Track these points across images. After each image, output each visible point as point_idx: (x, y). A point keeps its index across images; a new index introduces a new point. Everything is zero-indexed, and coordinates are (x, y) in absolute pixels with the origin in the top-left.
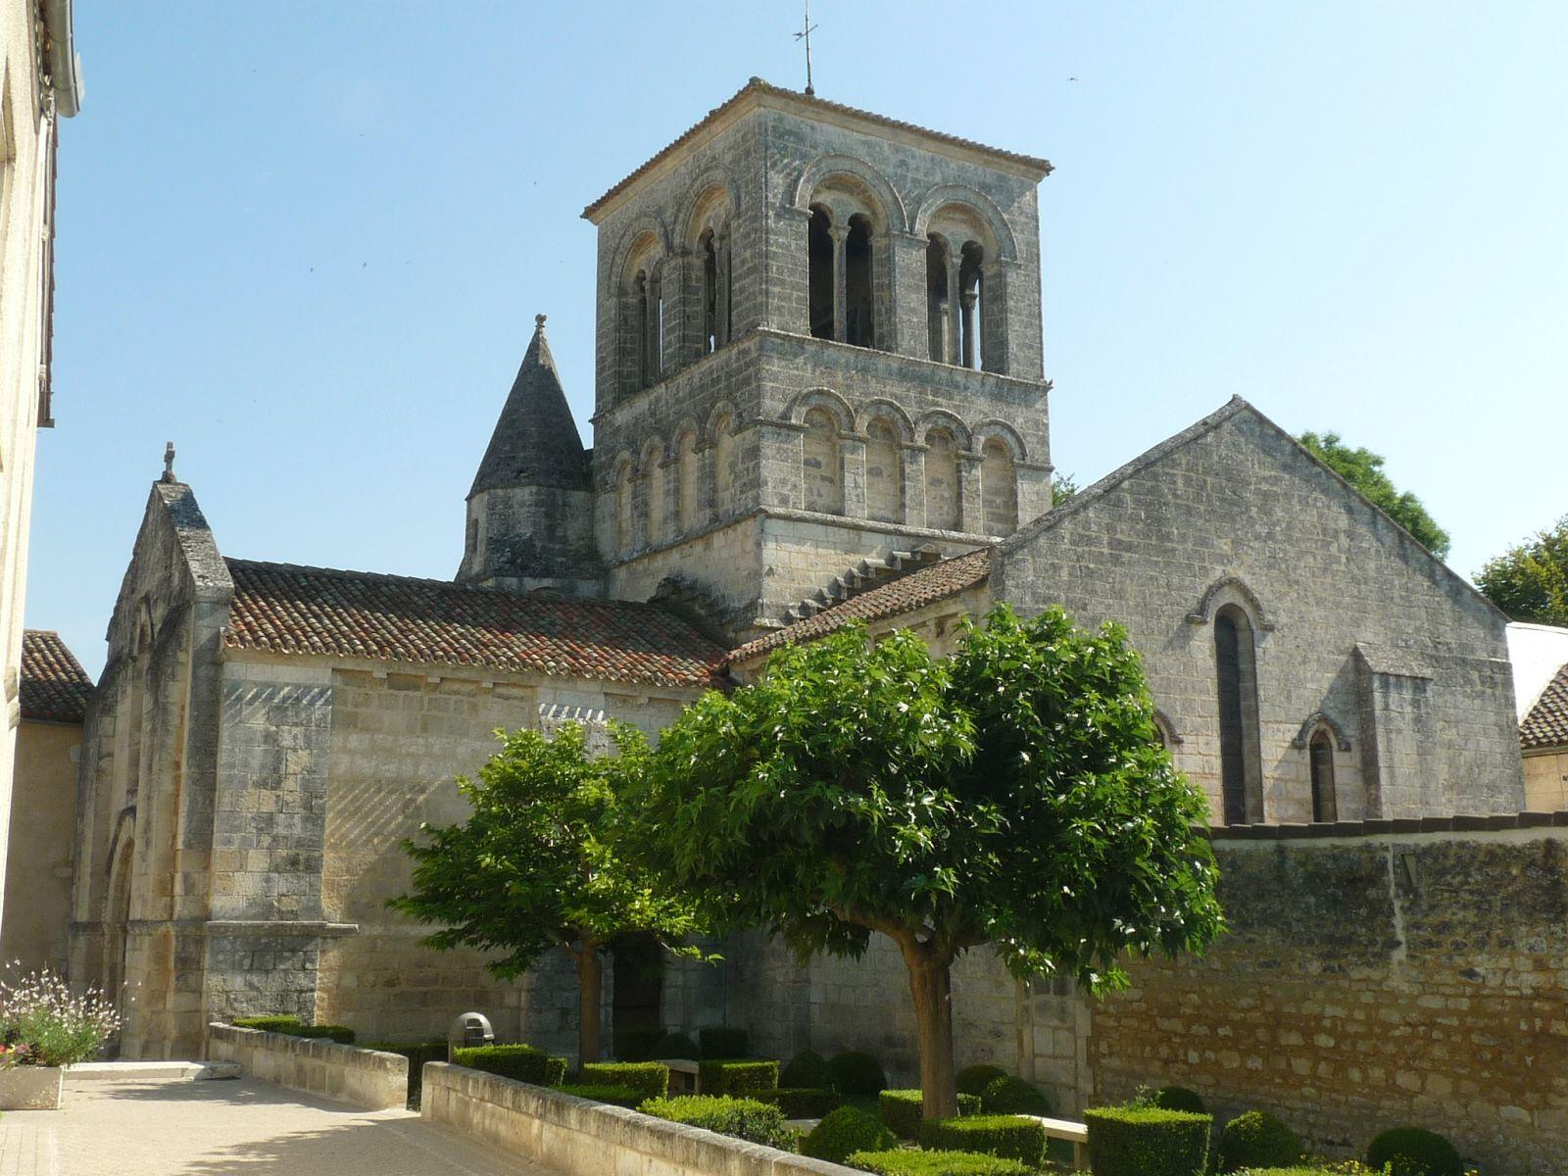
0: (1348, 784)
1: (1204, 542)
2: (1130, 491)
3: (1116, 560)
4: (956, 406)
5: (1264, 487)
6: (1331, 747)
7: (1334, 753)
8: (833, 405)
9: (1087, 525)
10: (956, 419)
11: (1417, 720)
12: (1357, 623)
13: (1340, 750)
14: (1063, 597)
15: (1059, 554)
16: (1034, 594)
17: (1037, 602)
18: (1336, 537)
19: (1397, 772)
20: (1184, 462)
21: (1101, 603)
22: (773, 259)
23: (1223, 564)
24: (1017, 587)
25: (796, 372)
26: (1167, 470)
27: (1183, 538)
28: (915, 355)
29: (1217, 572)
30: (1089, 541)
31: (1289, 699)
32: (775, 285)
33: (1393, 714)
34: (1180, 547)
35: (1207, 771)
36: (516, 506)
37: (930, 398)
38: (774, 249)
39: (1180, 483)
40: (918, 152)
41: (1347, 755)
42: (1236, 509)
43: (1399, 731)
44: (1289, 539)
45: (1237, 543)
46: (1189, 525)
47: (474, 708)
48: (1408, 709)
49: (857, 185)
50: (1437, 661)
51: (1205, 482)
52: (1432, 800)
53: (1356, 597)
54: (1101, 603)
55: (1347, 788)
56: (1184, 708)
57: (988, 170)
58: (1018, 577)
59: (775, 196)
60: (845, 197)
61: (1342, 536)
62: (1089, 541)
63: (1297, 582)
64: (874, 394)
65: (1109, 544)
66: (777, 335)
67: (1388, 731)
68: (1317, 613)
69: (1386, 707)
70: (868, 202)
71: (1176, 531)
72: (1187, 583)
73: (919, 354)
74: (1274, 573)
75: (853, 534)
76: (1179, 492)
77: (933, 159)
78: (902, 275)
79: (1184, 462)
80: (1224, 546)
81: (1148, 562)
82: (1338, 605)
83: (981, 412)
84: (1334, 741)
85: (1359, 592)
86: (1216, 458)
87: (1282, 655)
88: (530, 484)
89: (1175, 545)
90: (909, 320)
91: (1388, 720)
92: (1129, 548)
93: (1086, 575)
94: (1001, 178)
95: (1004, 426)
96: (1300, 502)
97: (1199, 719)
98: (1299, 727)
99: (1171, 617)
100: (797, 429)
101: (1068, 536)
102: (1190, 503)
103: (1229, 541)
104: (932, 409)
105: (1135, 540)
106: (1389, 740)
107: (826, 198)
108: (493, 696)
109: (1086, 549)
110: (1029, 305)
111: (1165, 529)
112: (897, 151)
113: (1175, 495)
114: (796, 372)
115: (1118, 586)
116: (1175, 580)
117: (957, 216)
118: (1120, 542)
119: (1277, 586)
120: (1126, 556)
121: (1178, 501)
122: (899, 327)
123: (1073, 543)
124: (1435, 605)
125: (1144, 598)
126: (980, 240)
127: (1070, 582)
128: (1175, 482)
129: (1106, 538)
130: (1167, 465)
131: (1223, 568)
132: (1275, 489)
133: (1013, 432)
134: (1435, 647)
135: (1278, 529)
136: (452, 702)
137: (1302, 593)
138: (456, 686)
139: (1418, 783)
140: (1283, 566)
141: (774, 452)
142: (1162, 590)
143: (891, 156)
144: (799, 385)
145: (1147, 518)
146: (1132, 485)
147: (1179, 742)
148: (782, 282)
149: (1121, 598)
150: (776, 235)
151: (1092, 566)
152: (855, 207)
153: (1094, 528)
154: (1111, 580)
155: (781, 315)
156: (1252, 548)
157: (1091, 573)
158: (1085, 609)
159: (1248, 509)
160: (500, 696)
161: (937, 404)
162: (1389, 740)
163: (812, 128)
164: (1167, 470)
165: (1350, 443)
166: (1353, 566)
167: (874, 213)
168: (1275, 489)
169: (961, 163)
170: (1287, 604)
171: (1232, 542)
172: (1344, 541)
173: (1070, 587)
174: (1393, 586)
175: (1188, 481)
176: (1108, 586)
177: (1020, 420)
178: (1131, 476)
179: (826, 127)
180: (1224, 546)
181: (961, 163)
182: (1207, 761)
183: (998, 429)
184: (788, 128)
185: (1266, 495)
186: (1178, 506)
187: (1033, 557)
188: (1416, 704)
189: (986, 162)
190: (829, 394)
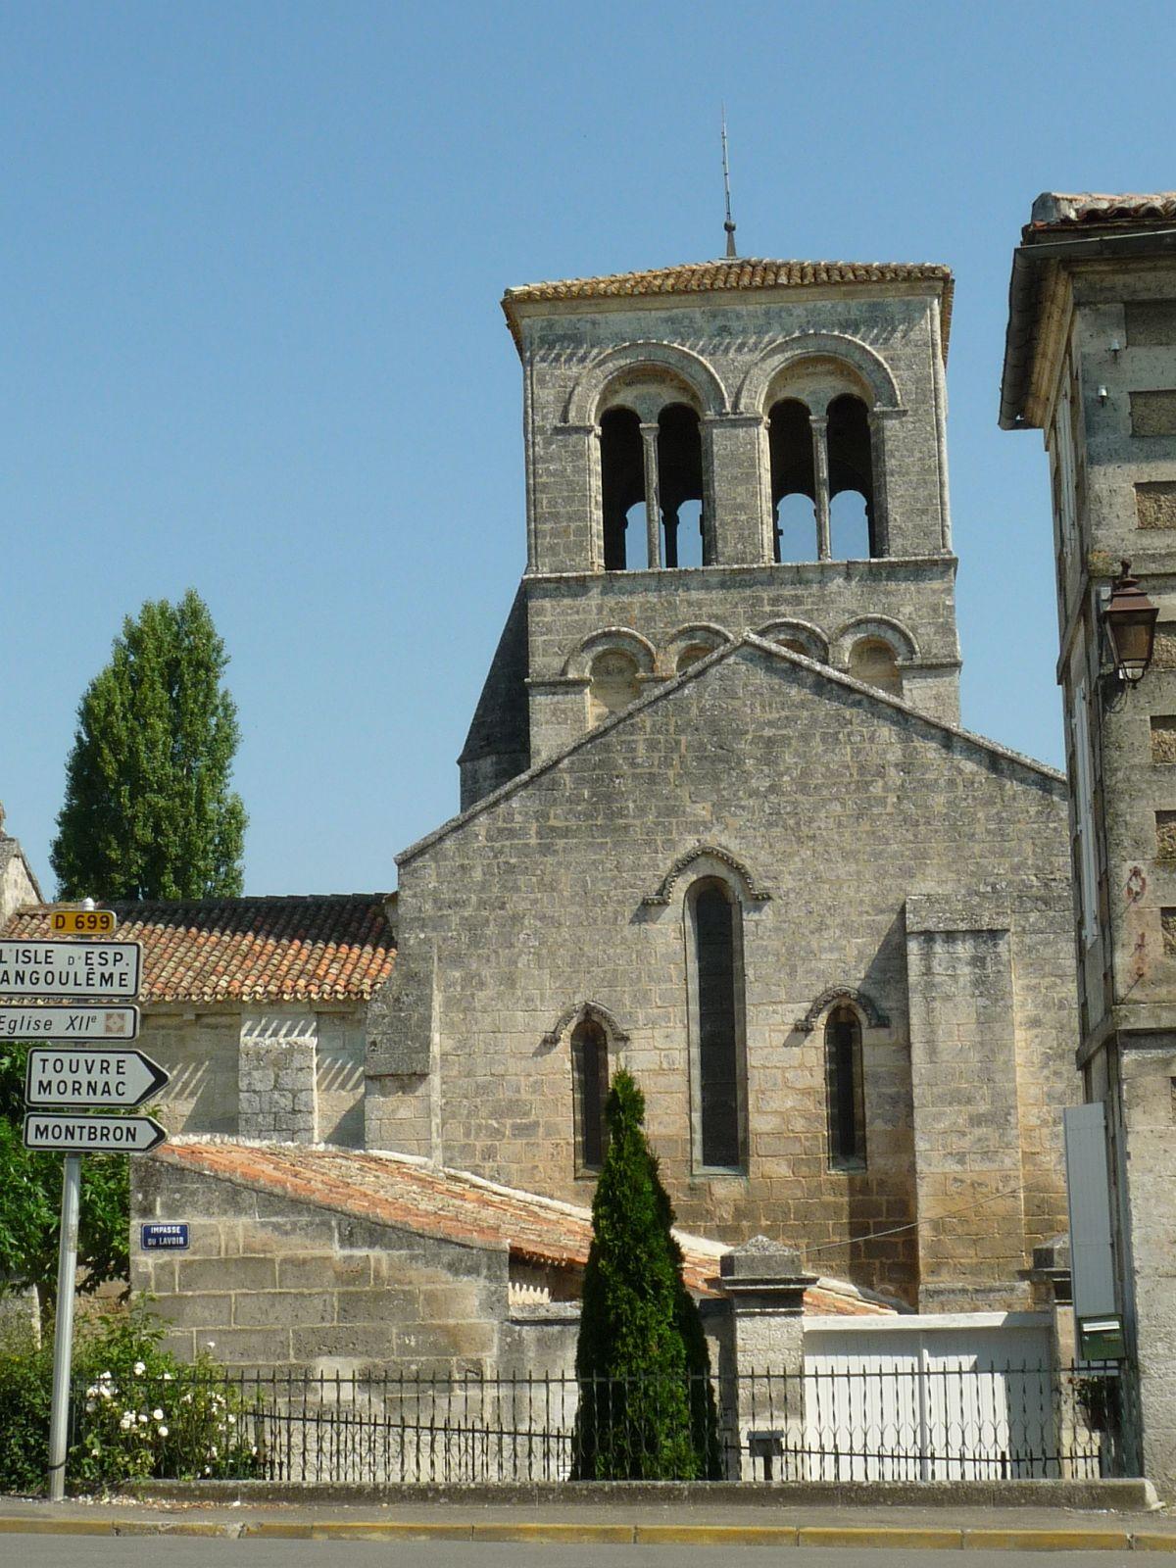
0: (882, 1066)
1: (671, 811)
2: (570, 770)
3: (546, 849)
4: (806, 612)
5: (768, 732)
6: (860, 1024)
7: (864, 1031)
8: (627, 646)
9: (509, 817)
10: (805, 628)
11: (979, 982)
12: (908, 874)
13: (870, 1026)
14: (474, 898)
15: (471, 854)
16: (435, 901)
17: (440, 909)
18: (881, 772)
19: (941, 1046)
20: (648, 725)
21: (524, 899)
22: (542, 492)
23: (698, 832)
24: (415, 896)
25: (576, 617)
26: (624, 738)
27: (642, 811)
28: (743, 561)
29: (690, 843)
30: (512, 833)
31: (793, 973)
32: (546, 521)
33: (938, 979)
34: (637, 822)
35: (665, 1066)
36: (481, 780)
37: (767, 609)
38: (544, 479)
39: (641, 749)
40: (742, 309)
41: (883, 1032)
42: (721, 766)
43: (948, 998)
44: (804, 789)
45: (719, 807)
46: (650, 794)
47: (182, 1040)
48: (965, 971)
49: (666, 371)
50: (1046, 903)
51: (678, 742)
52: (998, 1077)
53: (911, 842)
54: (524, 899)
55: (879, 1070)
56: (635, 999)
57: (853, 303)
58: (417, 885)
59: (544, 418)
60: (653, 389)
61: (892, 771)
62: (512, 833)
63: (813, 838)
64: (684, 621)
65: (538, 833)
66: (548, 580)
67: (928, 1000)
68: (843, 869)
69: (928, 971)
70: (684, 388)
71: (631, 805)
72: (645, 859)
73: (749, 557)
74: (777, 831)
75: (460, 834)
76: (639, 760)
77: (767, 313)
78: (723, 466)
79: (648, 725)
80: (702, 811)
81: (591, 844)
82: (877, 855)
83: (844, 611)
84: (862, 1017)
85: (915, 836)
86: (694, 711)
87: (785, 926)
88: (489, 754)
89: (630, 821)
90: (735, 520)
91: (930, 986)
92: (566, 833)
93: (505, 872)
94: (874, 306)
95: (881, 622)
96: (824, 740)
97: (655, 1010)
98: (808, 1005)
99: (619, 902)
100: (579, 684)
101: (483, 832)
102: (655, 770)
103: (708, 805)
104: (771, 622)
105: (573, 823)
106: (930, 1011)
107: (626, 398)
108: (201, 1027)
109: (508, 843)
110: (920, 459)
111: (615, 806)
112: (715, 317)
113: (633, 765)
114: (576, 617)
115: (547, 879)
116: (629, 859)
117: (820, 368)
118: (553, 829)
119: (780, 846)
120: (561, 843)
121: (638, 771)
122: (719, 531)
123: (489, 838)
124: (1048, 833)
125: (585, 886)
126: (855, 390)
127: (484, 882)
128: (633, 750)
129: (534, 827)
130: (624, 732)
131: (696, 837)
132: (784, 732)
133: (894, 627)
134: (1046, 885)
135: (786, 778)
136: (160, 1038)
137: (820, 849)
138: (163, 1021)
139: (974, 1057)
140: (791, 822)
141: (548, 716)
142: (609, 874)
143: (705, 325)
144: (580, 631)
145: (594, 795)
146: (573, 763)
147: (625, 1039)
148: (555, 516)
149: (553, 890)
150: (545, 462)
151: (513, 861)
152: (667, 396)
153: (518, 818)
154: (539, 872)
155: (555, 554)
156: (743, 808)
157: (511, 869)
158: (502, 908)
159: (740, 762)
160: (208, 1026)
161: (778, 615)
162: (930, 1011)
163: (594, 323)
164: (624, 738)
165: (50, 851)
166: (907, 805)
167: (694, 397)
168: (784, 732)
169: (810, 305)
170: (796, 864)
171: (713, 806)
172: (895, 777)
173: (484, 886)
174: (974, 820)
175: (652, 746)
176: (534, 879)
177: (907, 610)
178: (570, 754)
179: (611, 317)
180: (702, 811)
181: (810, 305)
182: (666, 1056)
183: (872, 627)
184: (561, 333)
185: (770, 742)
186: (635, 776)
187: (437, 862)
188: (978, 961)
189: (847, 294)
190: (618, 634)
